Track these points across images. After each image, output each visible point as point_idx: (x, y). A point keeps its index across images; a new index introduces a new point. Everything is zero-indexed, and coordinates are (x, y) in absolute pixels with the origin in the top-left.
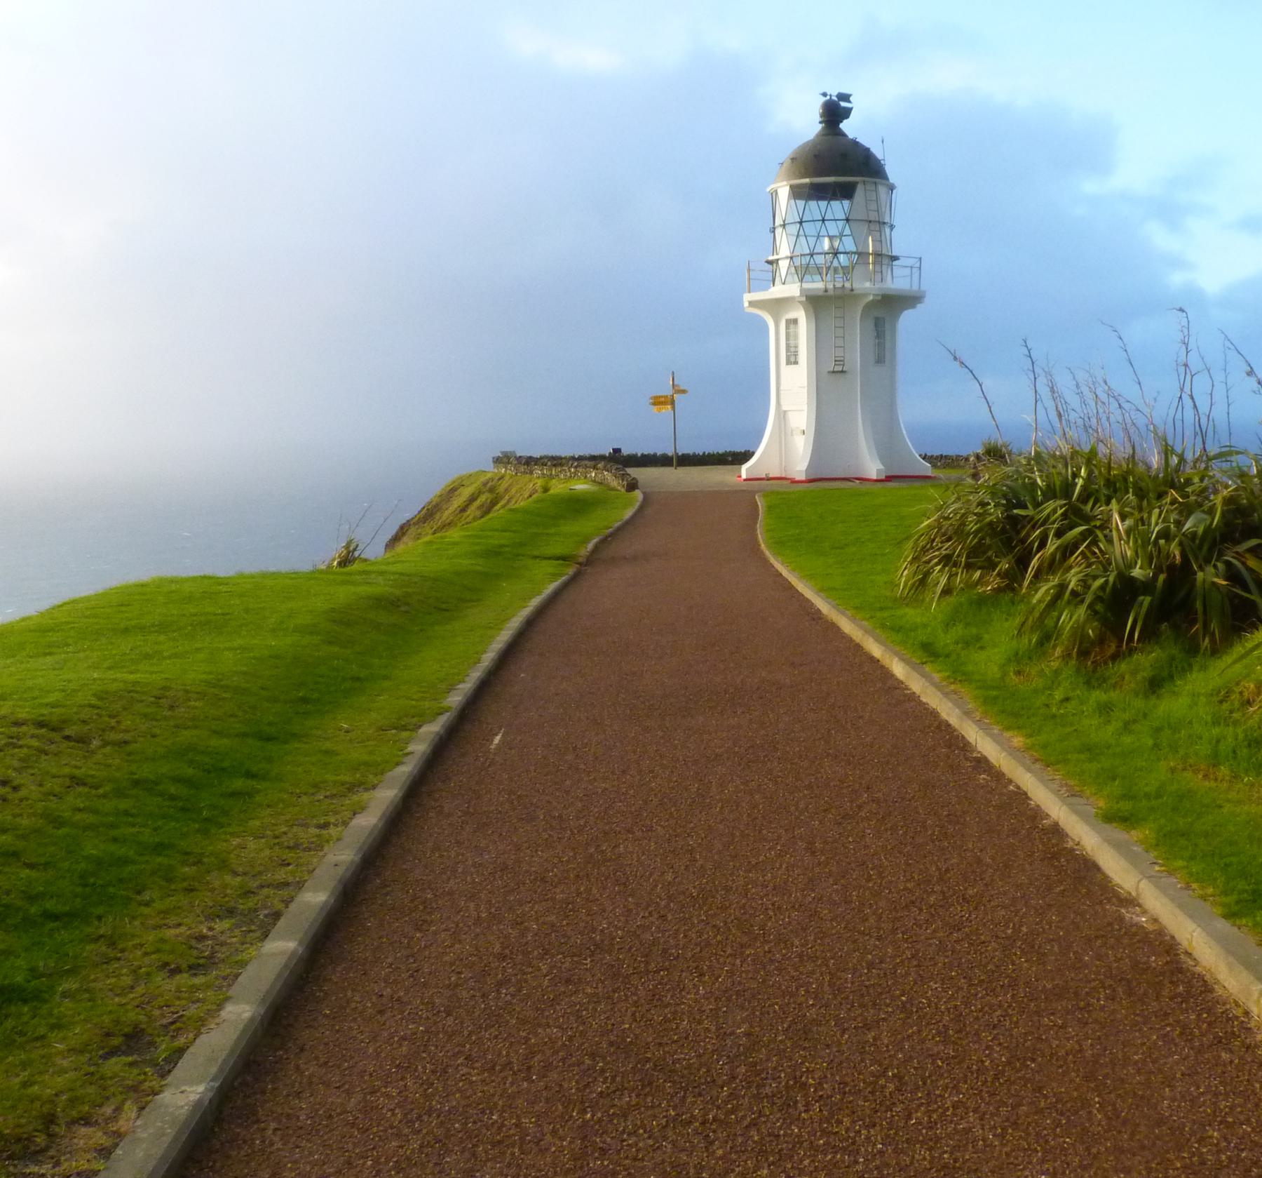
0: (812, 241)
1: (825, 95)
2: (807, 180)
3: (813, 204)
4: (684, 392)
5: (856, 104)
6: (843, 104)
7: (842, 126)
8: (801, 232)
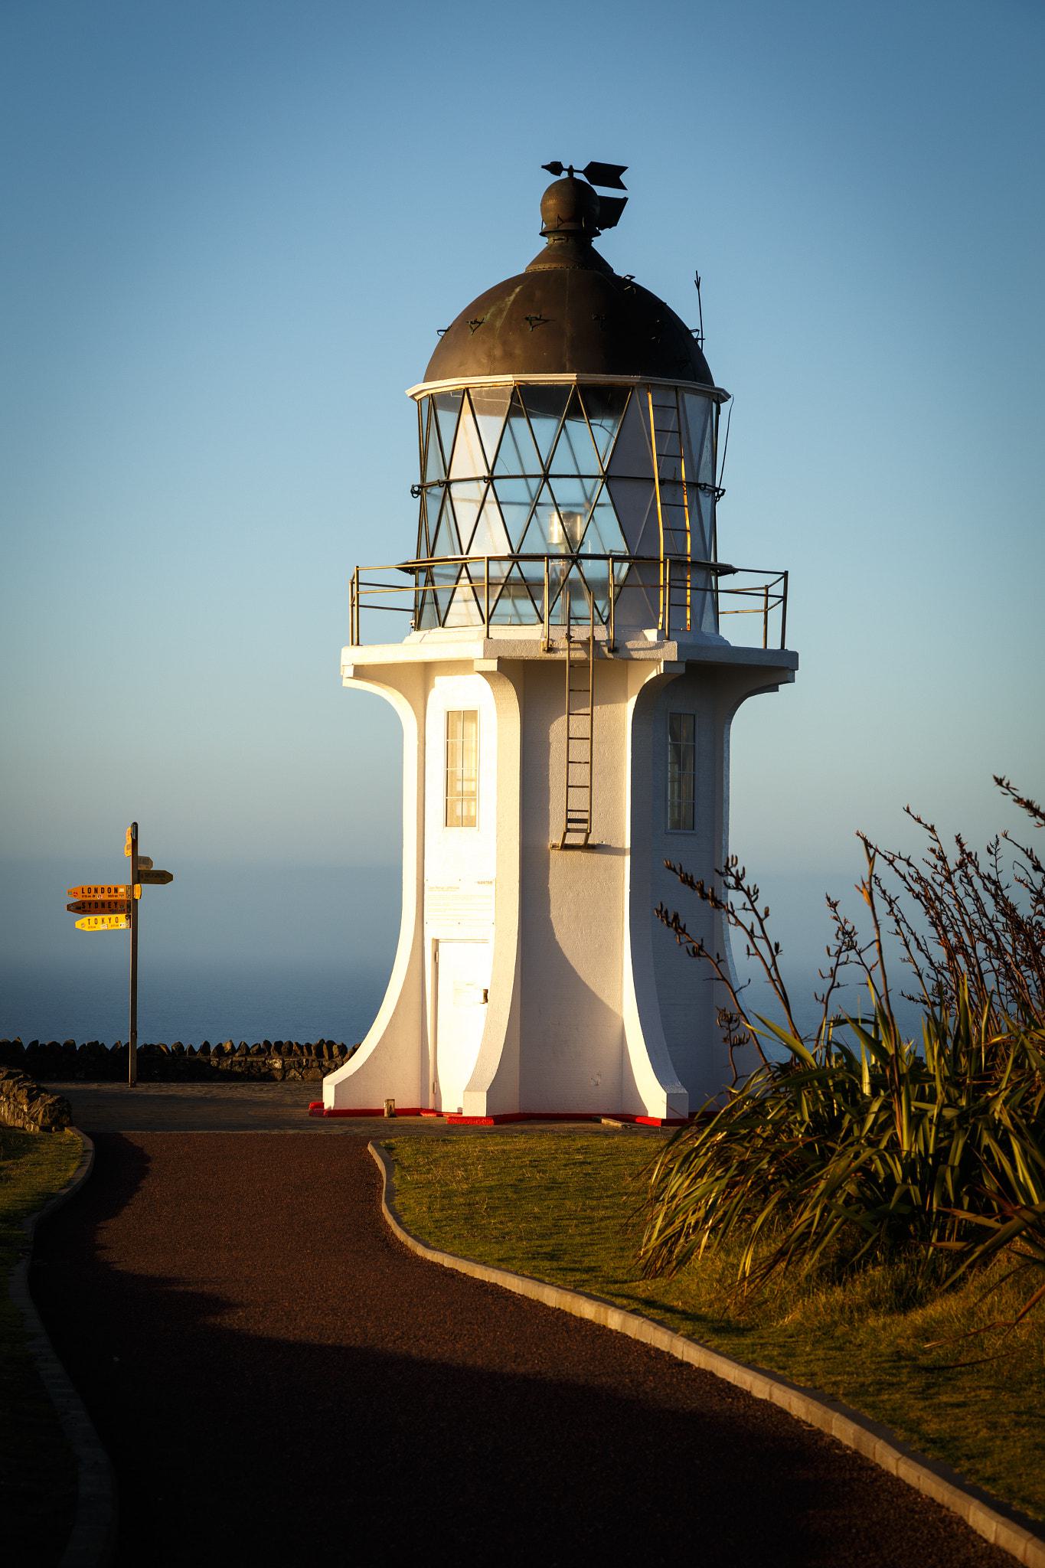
0: (517, 516)
1: (555, 168)
2: (509, 379)
3: (577, 428)
4: (164, 877)
5: (634, 187)
6: (602, 191)
7: (598, 244)
8: (545, 497)
